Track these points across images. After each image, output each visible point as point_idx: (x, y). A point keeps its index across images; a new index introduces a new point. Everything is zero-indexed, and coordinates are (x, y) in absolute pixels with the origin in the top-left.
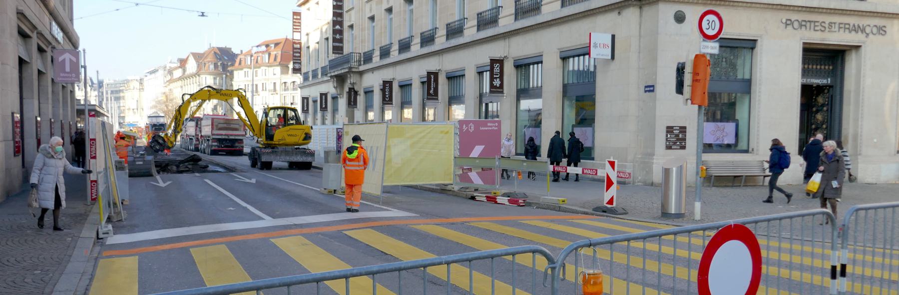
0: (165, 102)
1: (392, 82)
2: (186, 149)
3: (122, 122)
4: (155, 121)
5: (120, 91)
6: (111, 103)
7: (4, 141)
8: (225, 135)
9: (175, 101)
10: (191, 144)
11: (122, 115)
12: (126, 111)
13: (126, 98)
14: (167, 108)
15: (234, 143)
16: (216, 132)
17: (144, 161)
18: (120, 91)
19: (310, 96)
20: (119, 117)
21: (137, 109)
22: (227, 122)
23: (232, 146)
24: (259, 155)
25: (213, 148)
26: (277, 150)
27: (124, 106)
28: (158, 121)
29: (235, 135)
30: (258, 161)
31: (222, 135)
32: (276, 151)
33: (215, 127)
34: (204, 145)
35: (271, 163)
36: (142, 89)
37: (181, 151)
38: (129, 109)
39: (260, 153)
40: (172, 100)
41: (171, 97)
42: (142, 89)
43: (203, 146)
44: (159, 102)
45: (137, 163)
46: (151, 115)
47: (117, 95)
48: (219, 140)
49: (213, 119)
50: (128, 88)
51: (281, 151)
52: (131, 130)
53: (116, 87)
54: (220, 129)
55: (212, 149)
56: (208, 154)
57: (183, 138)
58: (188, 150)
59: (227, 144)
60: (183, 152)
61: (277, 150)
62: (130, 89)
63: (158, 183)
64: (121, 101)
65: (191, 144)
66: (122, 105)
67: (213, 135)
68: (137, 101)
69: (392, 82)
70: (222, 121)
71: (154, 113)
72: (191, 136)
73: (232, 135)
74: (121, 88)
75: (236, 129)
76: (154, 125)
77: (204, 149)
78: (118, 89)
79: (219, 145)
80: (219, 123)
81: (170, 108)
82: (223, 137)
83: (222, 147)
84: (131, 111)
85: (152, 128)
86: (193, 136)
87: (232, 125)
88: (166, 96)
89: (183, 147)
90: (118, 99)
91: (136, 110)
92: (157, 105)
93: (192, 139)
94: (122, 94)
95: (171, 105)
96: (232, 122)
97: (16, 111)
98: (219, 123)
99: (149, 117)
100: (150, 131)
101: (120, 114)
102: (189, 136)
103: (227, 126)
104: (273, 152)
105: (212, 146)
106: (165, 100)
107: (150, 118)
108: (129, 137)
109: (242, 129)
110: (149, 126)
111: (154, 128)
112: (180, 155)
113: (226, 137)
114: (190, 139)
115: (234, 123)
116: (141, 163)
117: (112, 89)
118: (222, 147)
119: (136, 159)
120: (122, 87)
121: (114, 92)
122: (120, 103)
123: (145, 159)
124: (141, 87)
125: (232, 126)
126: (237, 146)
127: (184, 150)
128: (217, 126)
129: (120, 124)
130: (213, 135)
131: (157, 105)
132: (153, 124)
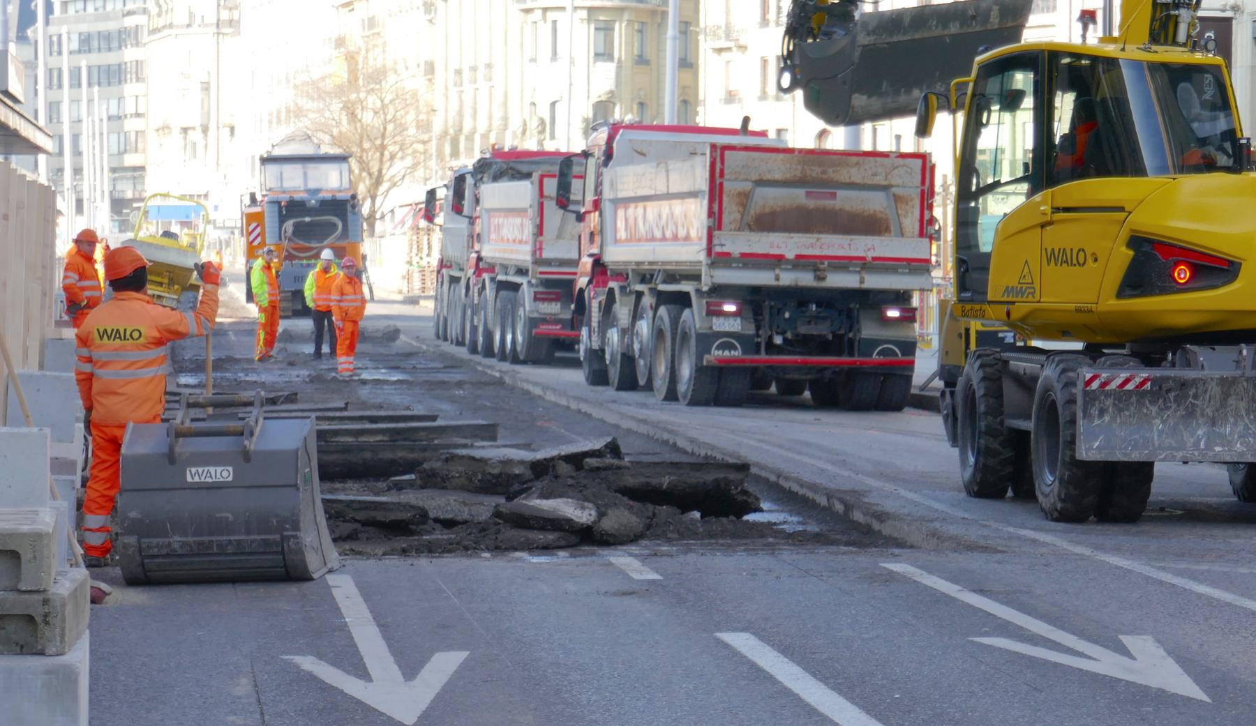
0: (340, 91)
1: (1228, 20)
2: (474, 350)
3: (129, 195)
4: (294, 181)
5: (123, 38)
6: (75, 101)
7: (997, 149)
8: (801, 262)
9: (391, 78)
10: (507, 315)
11: (130, 160)
12: (152, 137)
13: (148, 71)
14: (352, 116)
15: (852, 321)
16: (736, 243)
17: (246, 456)
18: (123, 38)
19: (1235, 8)
20: (113, 170)
21: (205, 130)
22: (815, 172)
23: (838, 344)
24: (1050, 411)
25: (716, 354)
26: (1190, 374)
27: (138, 115)
28: (312, 185)
29: (866, 265)
30: (1039, 451)
31: (775, 261)
32: (1183, 385)
33: (731, 213)
34: (628, 332)
35: (1144, 470)
36: (231, 22)
37: (443, 356)
38: (165, 128)
39: (1059, 397)
40: (377, 77)
41: (375, 60)
42: (231, 22)
43: (613, 335)
44: (316, 90)
45: (195, 475)
46: (277, 152)
47: (110, 58)
48: (753, 299)
49: (720, 153)
50: (160, 22)
51: (1223, 381)
52: (167, 234)
53: (107, 17)
54: (766, 223)
55: (709, 359)
56: (672, 396)
57: (454, 280)
58: (489, 352)
59: (803, 330)
60: (453, 364)
61: (1190, 374)
62: (171, 26)
63: (362, 673)
64: (130, 89)
65: (507, 315)
66: (129, 108)
67: (719, 259)
68: (206, 87)
69: (1228, 20)
70: (777, 168)
71: (290, 139)
72: (505, 268)
73: (842, 263)
74: (129, 22)
75: (872, 225)
76: (290, 208)
77: (628, 360)
78: (112, 26)
79: (751, 330)
80: (760, 183)
81: (367, 118)
82: (787, 278)
83: (771, 347)
84: (177, 136)
85: (282, 219)
86: (521, 272)
87: (841, 193)
88: (351, 58)
89: (453, 331)
90: (112, 76)
91: (195, 136)
92: (308, 104)
93: (515, 287)
94: (130, 54)
95: (373, 101)
96: (843, 175)
97: (1235, 356)
98: (760, 183)
99: (266, 160)
100: (270, 239)
101: (121, 153)
102: (491, 269)
103: (812, 204)
104: (1158, 392)
105: (706, 340)
106: (343, 76)
107: (273, 168)
108: (175, 276)
109: (911, 222)
110: (267, 209)
111: (289, 225)
112: (443, 384)
113: (806, 279)
114: (502, 286)
115: (856, 176)
116: (223, 474)
117: (84, 28)
118: (771, 347)
119: (185, 447)
120: (130, 13)
121: (95, 44)
122: (120, 99)
123: (252, 445)
124: (225, 15)
125: (846, 200)
126: (874, 343)
127: (462, 352)
128: (744, 199)
129: (118, 205)
130: (719, 259)
131: (308, 104)
132: (284, 198)
